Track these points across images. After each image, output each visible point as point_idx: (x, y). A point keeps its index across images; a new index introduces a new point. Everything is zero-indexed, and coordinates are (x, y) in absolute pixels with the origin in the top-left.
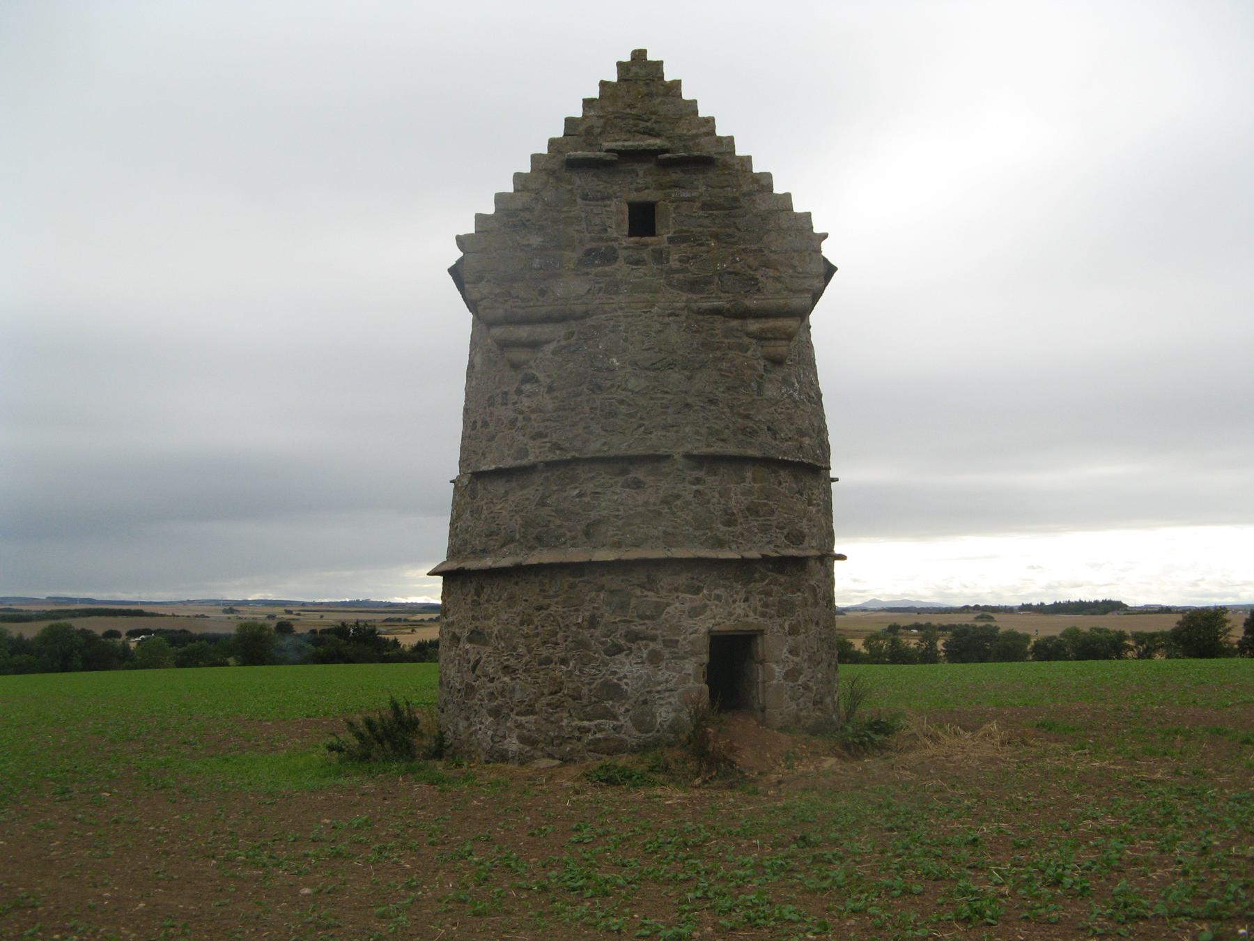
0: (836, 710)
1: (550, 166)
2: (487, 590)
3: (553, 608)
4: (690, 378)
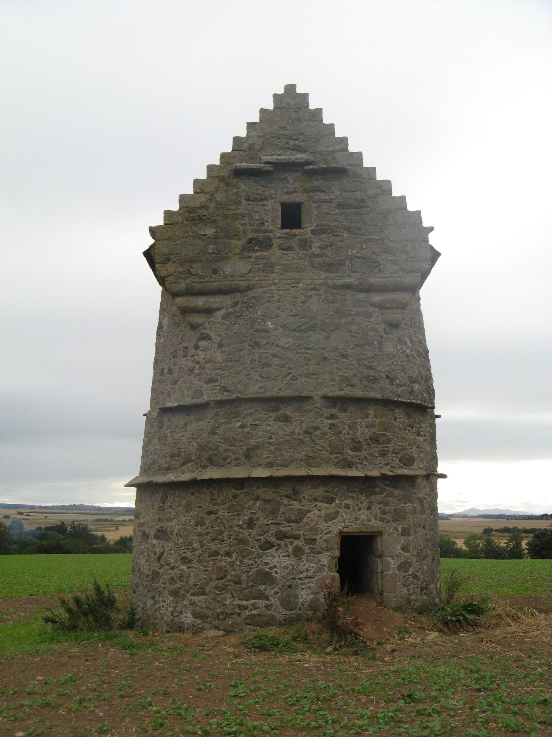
0: (439, 593)
1: (221, 174)
2: (170, 499)
3: (220, 513)
4: (327, 338)
